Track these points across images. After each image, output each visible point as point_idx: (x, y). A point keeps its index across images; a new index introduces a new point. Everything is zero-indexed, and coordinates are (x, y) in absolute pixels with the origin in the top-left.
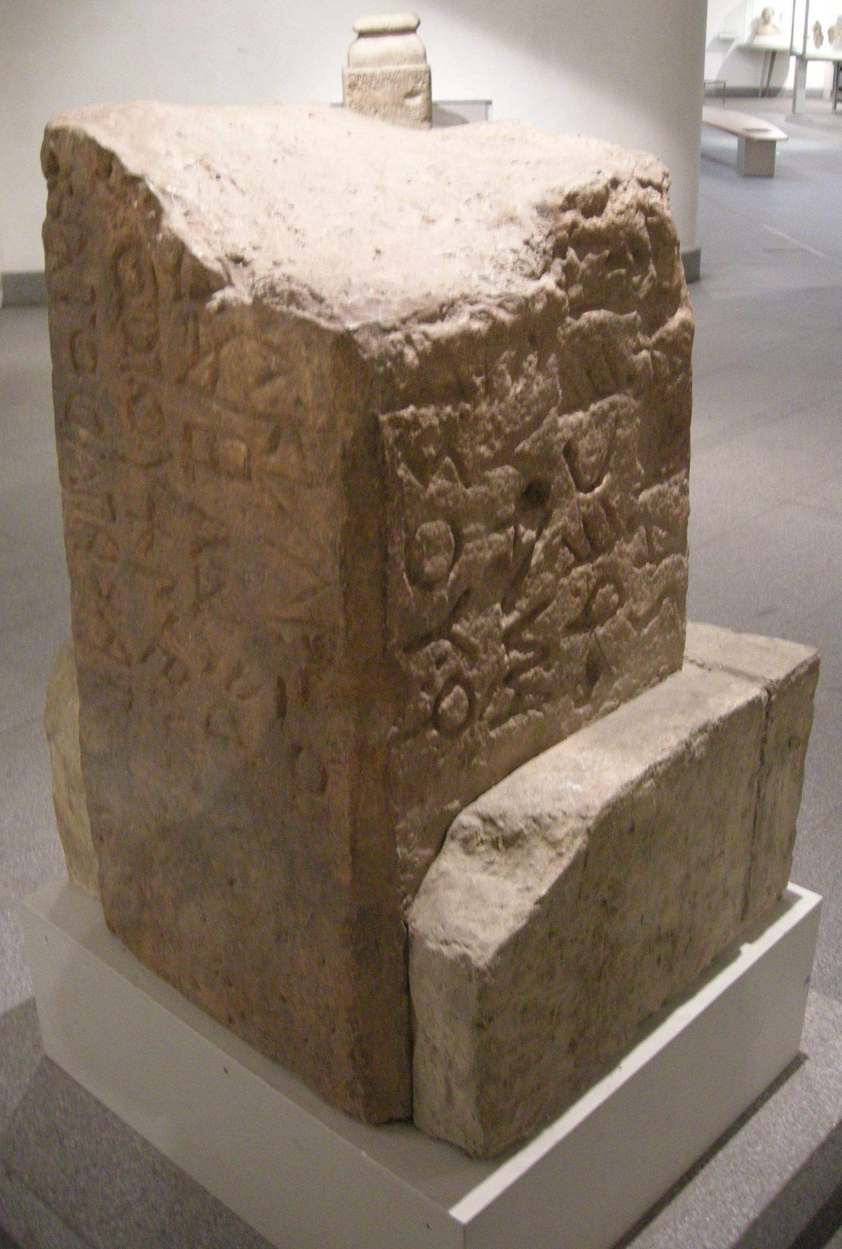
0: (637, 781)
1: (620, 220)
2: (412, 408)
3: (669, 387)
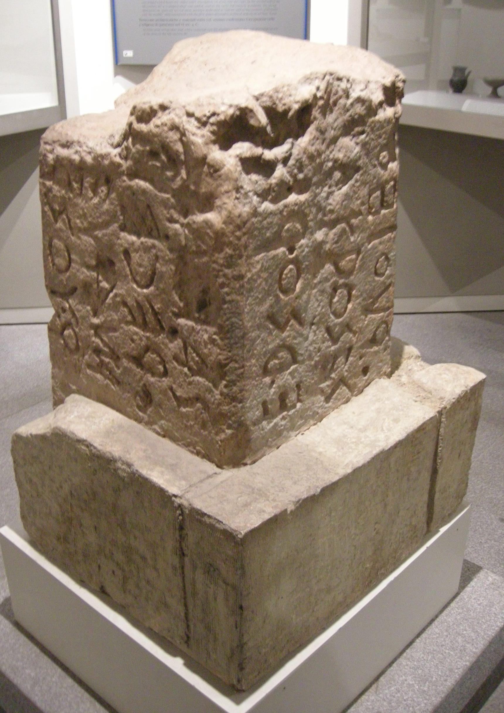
0: (79, 438)
1: (155, 130)
2: (51, 183)
3: (196, 260)
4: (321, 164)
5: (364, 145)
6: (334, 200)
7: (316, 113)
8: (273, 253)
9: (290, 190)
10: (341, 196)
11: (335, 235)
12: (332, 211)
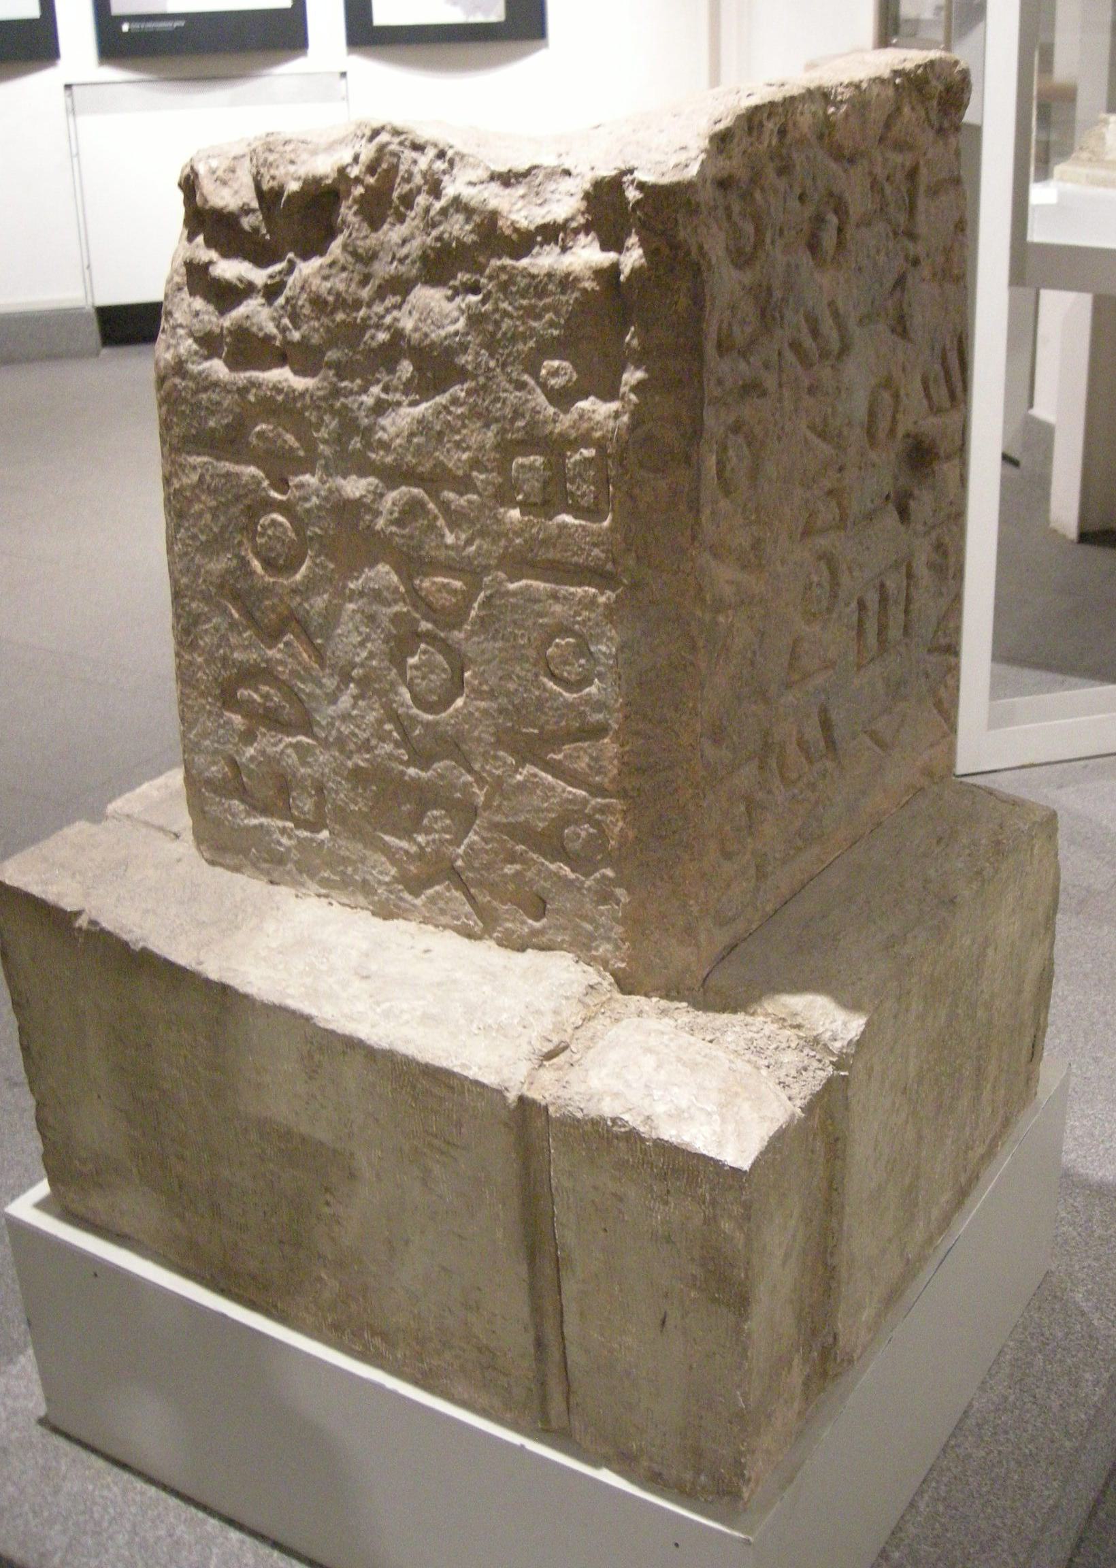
4: (364, 326)
5: (475, 320)
6: (394, 423)
7: (347, 212)
8: (227, 466)
9: (282, 357)
10: (409, 420)
11: (394, 504)
12: (385, 446)
